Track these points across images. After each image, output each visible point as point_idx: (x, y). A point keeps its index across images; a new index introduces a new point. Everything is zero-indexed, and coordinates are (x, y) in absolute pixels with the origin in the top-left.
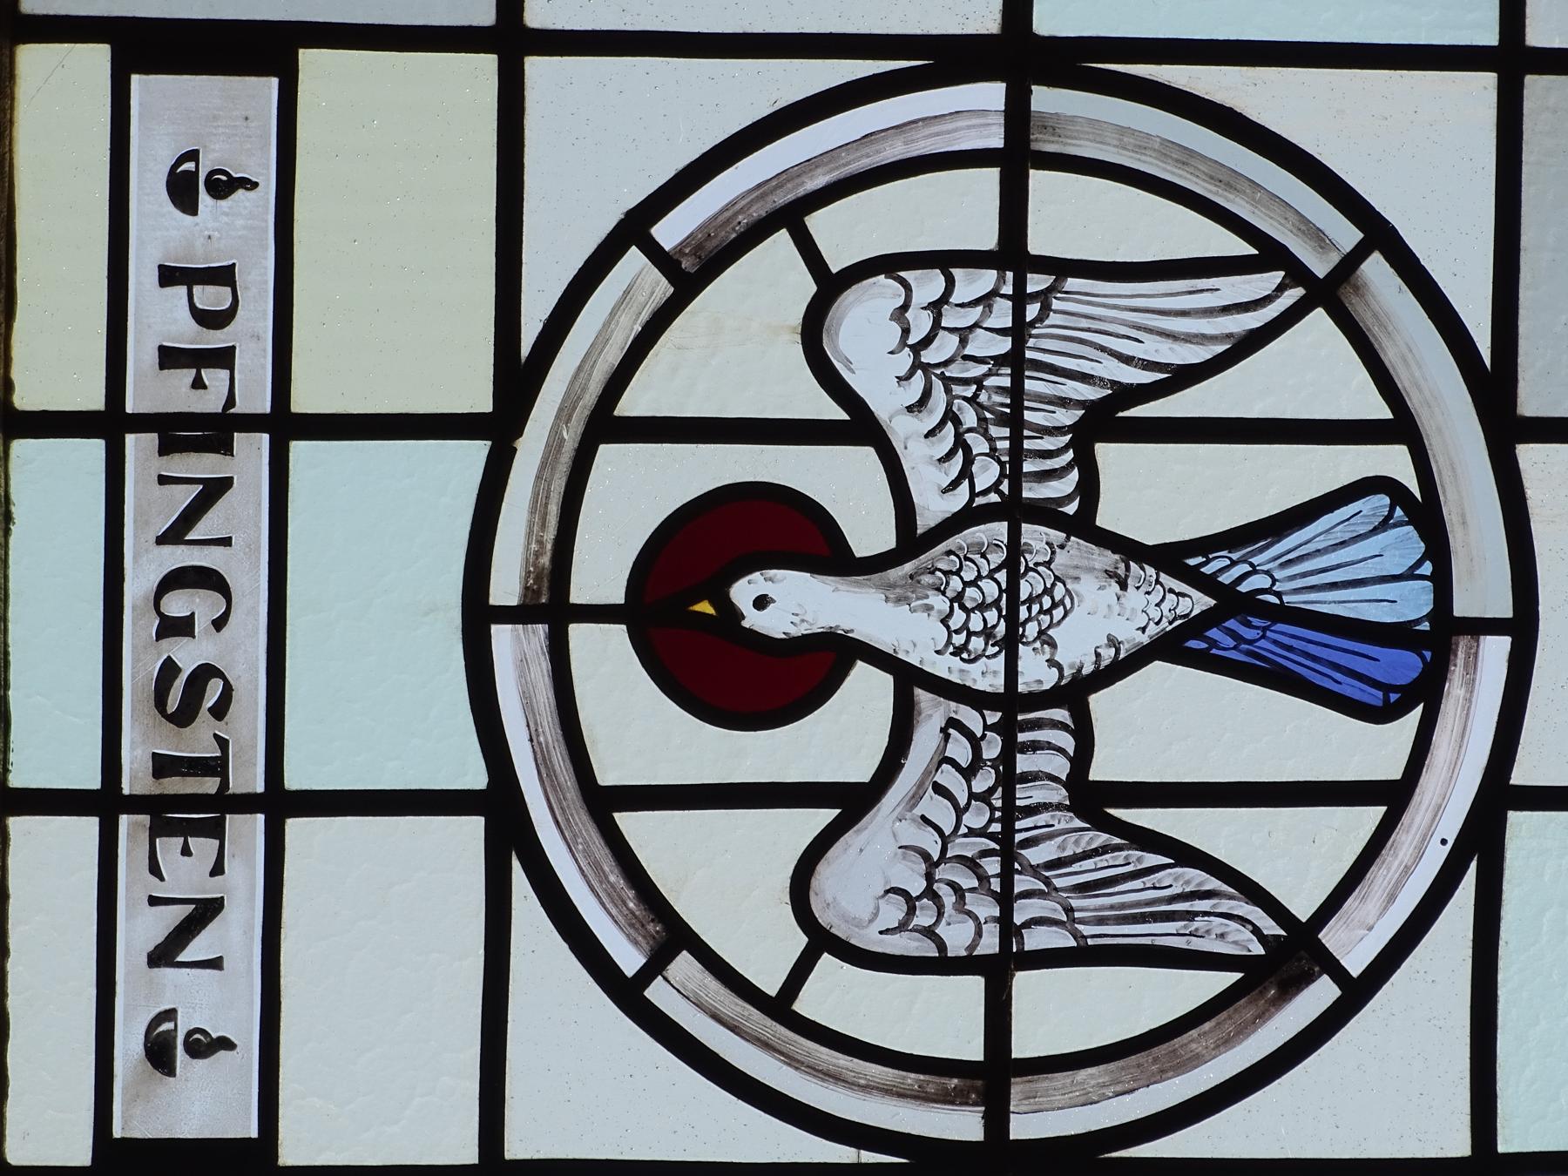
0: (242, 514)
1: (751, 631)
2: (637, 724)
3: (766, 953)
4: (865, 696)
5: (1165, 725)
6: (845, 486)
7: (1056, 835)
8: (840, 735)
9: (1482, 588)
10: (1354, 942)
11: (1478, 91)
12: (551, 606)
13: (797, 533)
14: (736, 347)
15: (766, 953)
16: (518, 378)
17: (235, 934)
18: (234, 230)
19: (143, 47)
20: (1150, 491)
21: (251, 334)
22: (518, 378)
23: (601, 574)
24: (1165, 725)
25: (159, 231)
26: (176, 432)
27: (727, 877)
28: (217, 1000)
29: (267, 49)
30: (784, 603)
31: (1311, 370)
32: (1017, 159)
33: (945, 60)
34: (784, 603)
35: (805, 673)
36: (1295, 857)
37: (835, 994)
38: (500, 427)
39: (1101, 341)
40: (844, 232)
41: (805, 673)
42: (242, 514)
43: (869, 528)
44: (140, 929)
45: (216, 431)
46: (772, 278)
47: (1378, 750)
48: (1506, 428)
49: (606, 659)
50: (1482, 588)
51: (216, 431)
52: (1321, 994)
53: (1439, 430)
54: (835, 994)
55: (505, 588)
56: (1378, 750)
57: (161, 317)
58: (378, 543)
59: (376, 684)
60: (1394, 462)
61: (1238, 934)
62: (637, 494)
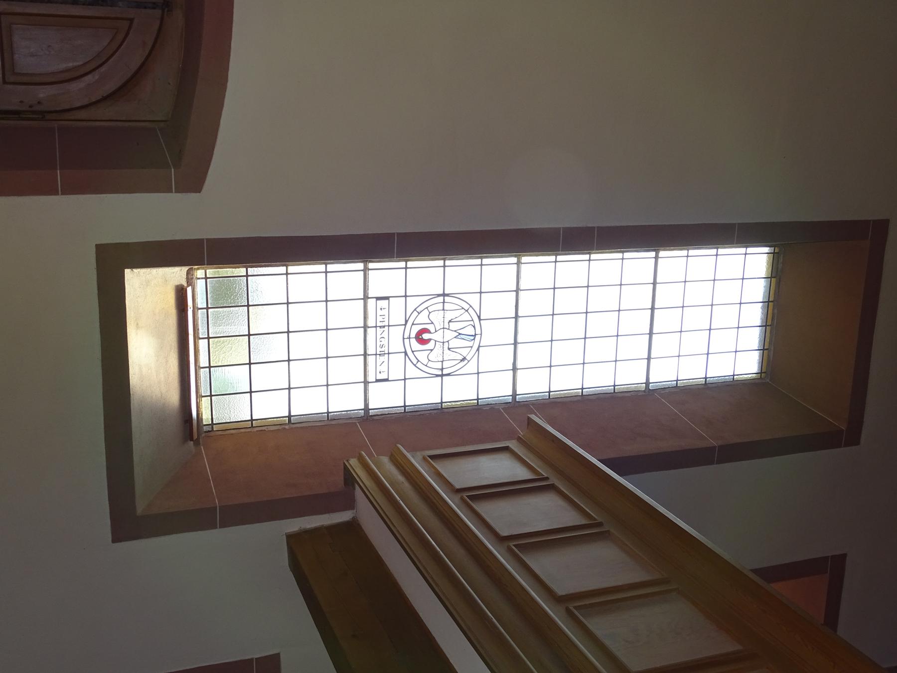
2: (416, 345)
3: (425, 361)
8: (430, 345)
9: (478, 332)
11: (250, 303)
12: (409, 338)
13: (426, 331)
15: (425, 361)
17: (386, 363)
20: (453, 326)
21: (386, 320)
23: (413, 335)
27: (422, 356)
29: (387, 298)
30: (425, 336)
31: (466, 317)
33: (439, 295)
34: (425, 336)
36: (464, 352)
37: (430, 364)
38: (405, 325)
40: (431, 309)
43: (432, 330)
45: (384, 327)
46: (426, 312)
47: (471, 344)
48: (480, 320)
49: (413, 341)
50: (478, 332)
51: (384, 327)
53: (31, 106)
54: (430, 364)
55: (418, 310)
56: (471, 344)
58: (396, 334)
59: (396, 345)
60: (472, 323)
61: (461, 358)
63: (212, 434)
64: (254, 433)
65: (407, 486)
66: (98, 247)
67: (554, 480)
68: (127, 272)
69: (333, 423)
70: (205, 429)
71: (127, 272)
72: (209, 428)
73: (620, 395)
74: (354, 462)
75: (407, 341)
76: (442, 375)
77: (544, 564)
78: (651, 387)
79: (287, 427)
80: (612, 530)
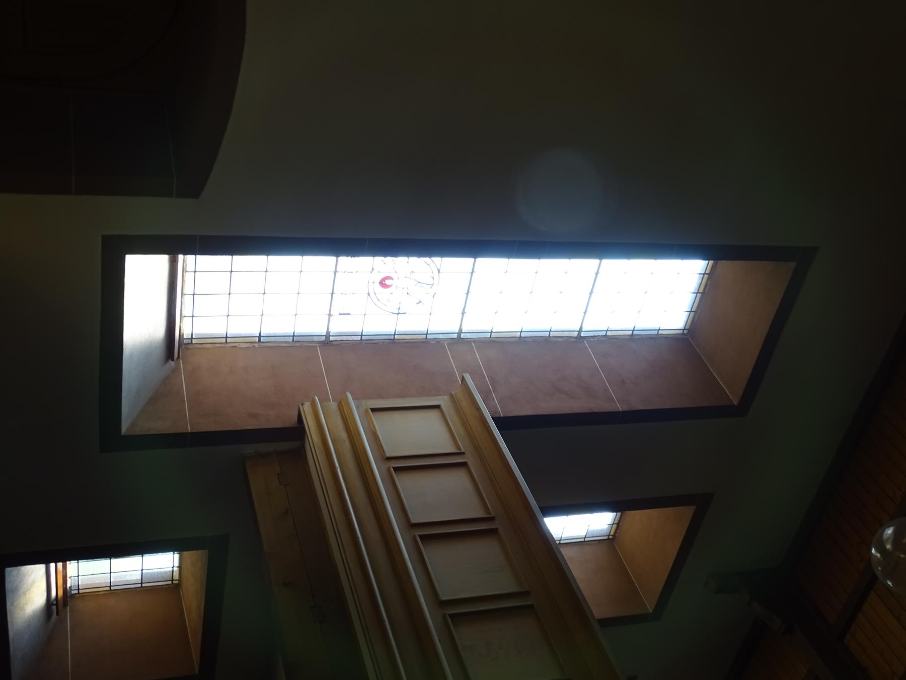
30: (388, 282)
34: (388, 282)
63: (190, 346)
64: (225, 347)
65: (347, 444)
66: (103, 236)
67: (469, 459)
68: (129, 258)
69: (297, 344)
70: (185, 341)
71: (129, 258)
72: (189, 341)
73: (554, 339)
74: (307, 409)
75: (371, 284)
76: (398, 314)
77: (439, 557)
78: (583, 334)
79: (256, 345)
80: (500, 530)
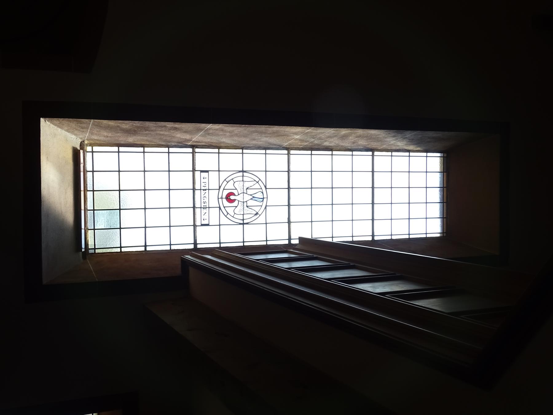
0: (207, 195)
1: (448, 217)
2: (226, 203)
3: (232, 214)
4: (236, 202)
5: (250, 203)
6: (235, 192)
7: (246, 208)
8: (235, 204)
9: (265, 196)
10: (260, 213)
12: (222, 198)
14: (230, 186)
15: (232, 214)
16: (220, 187)
18: (206, 180)
19: (202, 171)
20: (249, 192)
21: (207, 185)
22: (220, 187)
23: (224, 196)
24: (250, 203)
25: (203, 180)
26: (203, 190)
27: (230, 210)
28: (206, 217)
29: (207, 171)
30: (232, 197)
31: (257, 186)
32: (243, 220)
34: (232, 197)
35: (233, 201)
36: (257, 209)
37: (235, 216)
39: (247, 185)
41: (233, 201)
42: (207, 194)
43: (236, 194)
44: (203, 214)
45: (206, 190)
46: (232, 182)
47: (261, 204)
49: (224, 200)
50: (265, 196)
51: (206, 190)
52: (258, 215)
54: (235, 216)
56: (261, 204)
57: (203, 184)
58: (214, 195)
59: (214, 202)
60: (261, 190)
61: (255, 213)
62: (226, 193)
